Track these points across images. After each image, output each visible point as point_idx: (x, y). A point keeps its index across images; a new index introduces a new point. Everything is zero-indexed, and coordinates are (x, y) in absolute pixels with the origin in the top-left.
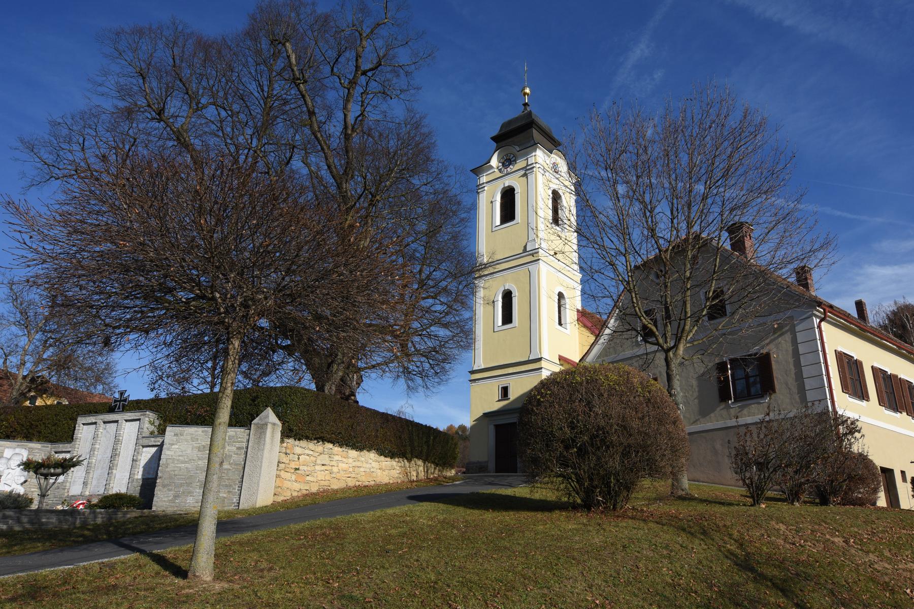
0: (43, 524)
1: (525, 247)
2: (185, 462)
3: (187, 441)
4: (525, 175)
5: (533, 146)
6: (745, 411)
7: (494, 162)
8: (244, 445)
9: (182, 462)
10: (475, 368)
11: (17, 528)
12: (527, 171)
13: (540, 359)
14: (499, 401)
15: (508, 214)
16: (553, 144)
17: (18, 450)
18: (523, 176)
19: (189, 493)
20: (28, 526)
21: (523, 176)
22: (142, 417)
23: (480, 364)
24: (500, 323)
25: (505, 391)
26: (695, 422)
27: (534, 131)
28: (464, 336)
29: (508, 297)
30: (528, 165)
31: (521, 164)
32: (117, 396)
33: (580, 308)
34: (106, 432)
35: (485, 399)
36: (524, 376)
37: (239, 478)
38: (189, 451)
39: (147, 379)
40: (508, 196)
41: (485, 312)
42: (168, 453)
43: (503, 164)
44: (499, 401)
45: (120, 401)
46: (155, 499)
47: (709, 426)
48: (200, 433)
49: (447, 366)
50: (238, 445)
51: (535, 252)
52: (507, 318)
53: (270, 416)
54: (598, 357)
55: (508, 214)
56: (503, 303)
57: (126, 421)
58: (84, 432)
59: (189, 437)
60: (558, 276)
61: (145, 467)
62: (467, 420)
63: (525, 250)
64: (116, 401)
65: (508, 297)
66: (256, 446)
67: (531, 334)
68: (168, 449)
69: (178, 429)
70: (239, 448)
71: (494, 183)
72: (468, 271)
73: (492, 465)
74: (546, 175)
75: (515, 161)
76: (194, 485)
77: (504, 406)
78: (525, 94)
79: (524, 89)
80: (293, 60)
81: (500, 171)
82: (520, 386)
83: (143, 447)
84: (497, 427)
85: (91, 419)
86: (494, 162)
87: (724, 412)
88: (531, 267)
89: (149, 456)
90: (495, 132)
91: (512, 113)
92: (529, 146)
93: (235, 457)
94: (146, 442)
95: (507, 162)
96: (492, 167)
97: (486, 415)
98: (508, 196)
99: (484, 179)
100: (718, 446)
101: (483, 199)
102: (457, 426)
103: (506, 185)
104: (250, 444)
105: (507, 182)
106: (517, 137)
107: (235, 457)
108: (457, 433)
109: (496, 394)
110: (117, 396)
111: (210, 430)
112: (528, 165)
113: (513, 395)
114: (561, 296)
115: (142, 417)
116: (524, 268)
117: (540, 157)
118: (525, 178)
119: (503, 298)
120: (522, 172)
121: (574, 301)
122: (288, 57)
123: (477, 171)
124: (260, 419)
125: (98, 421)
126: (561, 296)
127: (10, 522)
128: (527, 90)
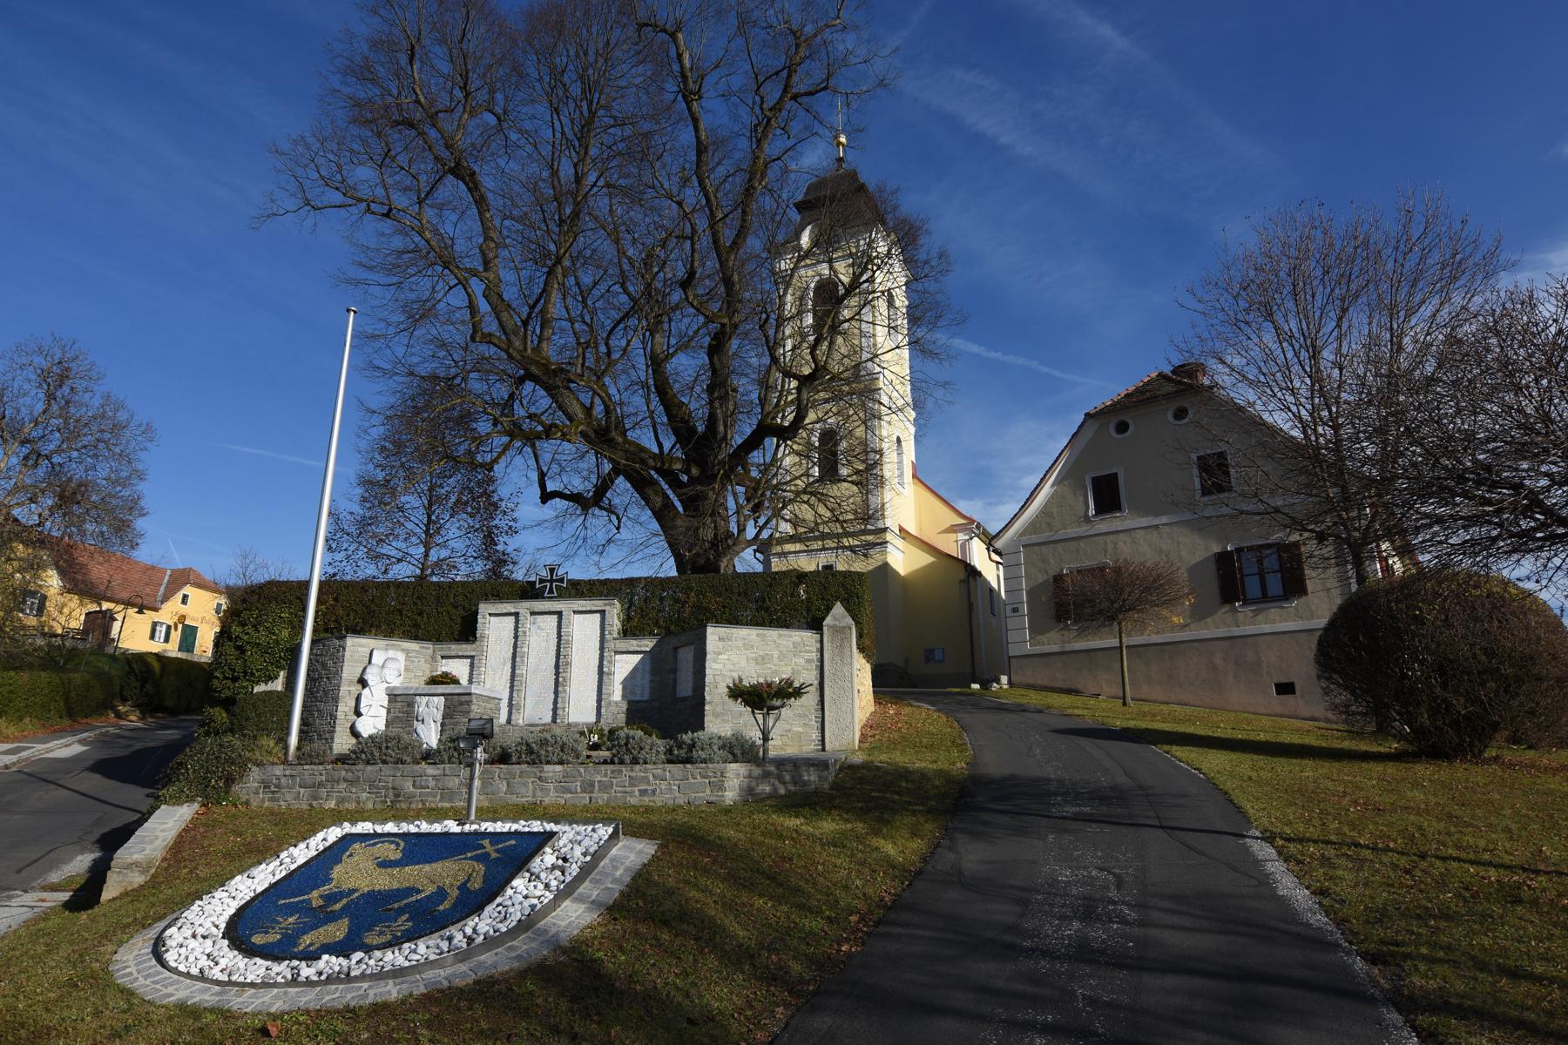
0: (805, 783)
6: (1260, 617)
17: (391, 653)
32: (544, 573)
34: (540, 633)
38: (743, 663)
42: (715, 666)
45: (551, 581)
47: (1205, 634)
53: (838, 615)
58: (495, 627)
59: (740, 643)
64: (541, 581)
66: (837, 659)
70: (808, 661)
78: (839, 143)
79: (837, 137)
83: (617, 653)
87: (1229, 618)
89: (630, 667)
100: (1218, 661)
104: (826, 655)
110: (544, 573)
111: (807, 637)
122: (680, 56)
124: (835, 619)
125: (522, 611)
126: (899, 440)
128: (843, 139)
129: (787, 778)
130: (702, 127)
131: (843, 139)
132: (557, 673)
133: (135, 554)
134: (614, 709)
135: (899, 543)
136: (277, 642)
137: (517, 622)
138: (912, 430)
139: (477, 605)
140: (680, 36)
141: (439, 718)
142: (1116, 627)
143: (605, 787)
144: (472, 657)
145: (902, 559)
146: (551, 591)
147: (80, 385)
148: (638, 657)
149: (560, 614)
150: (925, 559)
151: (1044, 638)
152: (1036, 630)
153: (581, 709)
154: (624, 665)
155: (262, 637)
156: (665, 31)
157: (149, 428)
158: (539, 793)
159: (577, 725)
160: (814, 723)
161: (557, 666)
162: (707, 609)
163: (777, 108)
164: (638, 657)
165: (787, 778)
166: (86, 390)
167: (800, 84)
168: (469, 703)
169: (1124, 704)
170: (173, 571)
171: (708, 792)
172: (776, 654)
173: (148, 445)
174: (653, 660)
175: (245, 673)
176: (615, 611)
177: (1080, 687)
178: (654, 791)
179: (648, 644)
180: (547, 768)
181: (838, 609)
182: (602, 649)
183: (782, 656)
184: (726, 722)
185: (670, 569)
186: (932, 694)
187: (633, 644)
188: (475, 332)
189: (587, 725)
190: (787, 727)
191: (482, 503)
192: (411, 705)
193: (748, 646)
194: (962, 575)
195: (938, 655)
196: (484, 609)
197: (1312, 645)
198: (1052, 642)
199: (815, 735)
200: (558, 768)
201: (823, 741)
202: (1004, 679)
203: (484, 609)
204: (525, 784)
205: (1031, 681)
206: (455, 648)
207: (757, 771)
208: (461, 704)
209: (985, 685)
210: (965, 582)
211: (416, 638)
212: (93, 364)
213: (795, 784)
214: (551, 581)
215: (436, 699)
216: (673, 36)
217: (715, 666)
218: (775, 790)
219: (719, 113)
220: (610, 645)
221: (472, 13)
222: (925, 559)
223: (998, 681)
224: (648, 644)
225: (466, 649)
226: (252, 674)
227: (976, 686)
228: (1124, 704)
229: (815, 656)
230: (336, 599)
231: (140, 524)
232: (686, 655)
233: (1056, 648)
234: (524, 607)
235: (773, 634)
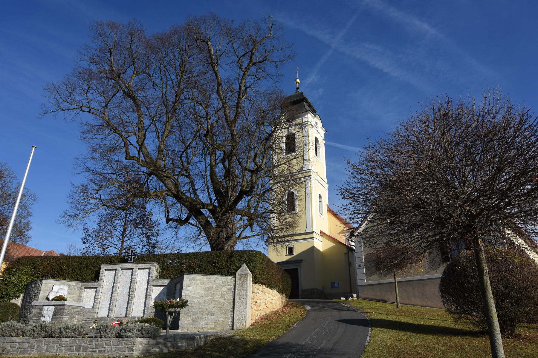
0: (179, 347)
2: (198, 298)
3: (197, 284)
5: (307, 112)
8: (232, 287)
9: (196, 298)
11: (165, 351)
12: (302, 126)
13: (313, 232)
16: (314, 112)
17: (62, 287)
19: (201, 318)
20: (171, 349)
22: (151, 267)
25: (291, 250)
26: (427, 273)
30: (303, 122)
31: (298, 121)
34: (124, 277)
37: (230, 307)
38: (199, 291)
39: (82, 236)
42: (186, 292)
44: (287, 255)
45: (131, 256)
46: (180, 322)
48: (205, 279)
50: (228, 287)
57: (139, 269)
58: (106, 275)
59: (198, 282)
61: (155, 299)
66: (241, 288)
68: (186, 290)
69: (191, 276)
70: (229, 289)
76: (204, 313)
78: (297, 82)
79: (296, 80)
80: (212, 51)
83: (154, 286)
85: (113, 267)
93: (227, 295)
94: (156, 283)
98: (291, 138)
107: (227, 295)
111: (229, 279)
113: (296, 252)
115: (151, 267)
117: (310, 117)
121: (326, 200)
122: (209, 50)
124: (242, 271)
125: (118, 269)
126: (320, 196)
127: (161, 346)
128: (298, 81)
129: (169, 345)
130: (219, 76)
131: (298, 81)
132: (129, 295)
133: (28, 245)
134: (150, 310)
135: (321, 238)
136: (21, 282)
137: (132, 272)
138: (327, 192)
139: (100, 266)
140: (209, 43)
141: (51, 315)
142: (393, 274)
143: (85, 349)
144: (96, 288)
145: (321, 245)
146: (131, 260)
147: (7, 180)
148: (162, 288)
149: (132, 269)
150: (330, 244)
151: (372, 278)
152: (369, 274)
153: (137, 311)
154: (156, 291)
155: (15, 280)
156: (204, 41)
157: (35, 196)
158: (58, 351)
159: (135, 317)
160: (230, 317)
161: (129, 292)
162: (193, 267)
163: (247, 68)
164: (162, 288)
165: (169, 345)
166: (10, 182)
167: (255, 58)
168: (63, 309)
169: (397, 307)
170: (46, 252)
171: (127, 351)
172: (214, 286)
173: (34, 202)
174: (168, 289)
175: (7, 295)
176: (155, 268)
177: (386, 299)
178: (104, 351)
179: (166, 282)
180: (63, 339)
181: (244, 266)
182: (148, 284)
183: (217, 287)
184: (189, 316)
185: (207, 248)
186: (324, 302)
187: (161, 282)
188: (127, 156)
189: (138, 318)
190: (217, 319)
191: (145, 223)
192: (41, 309)
193: (202, 283)
194: (345, 251)
195: (336, 285)
196: (103, 267)
197: (439, 281)
198: (375, 280)
199: (230, 322)
200: (68, 340)
201: (233, 325)
202: (355, 295)
203: (103, 267)
204: (54, 347)
205: (367, 296)
206: (90, 284)
207: (152, 342)
208: (61, 310)
209: (347, 299)
210: (347, 254)
211: (77, 280)
212: (13, 172)
213: (173, 347)
214: (131, 256)
215: (51, 307)
216: (207, 43)
217: (186, 292)
218: (162, 351)
219: (226, 72)
220: (151, 283)
221: (135, 40)
222: (330, 244)
223: (352, 297)
224: (166, 282)
225: (94, 284)
226: (10, 295)
227: (343, 299)
228: (397, 307)
229: (232, 287)
230: (48, 264)
231: (29, 233)
232: (178, 286)
233: (376, 282)
234: (119, 266)
235: (214, 278)
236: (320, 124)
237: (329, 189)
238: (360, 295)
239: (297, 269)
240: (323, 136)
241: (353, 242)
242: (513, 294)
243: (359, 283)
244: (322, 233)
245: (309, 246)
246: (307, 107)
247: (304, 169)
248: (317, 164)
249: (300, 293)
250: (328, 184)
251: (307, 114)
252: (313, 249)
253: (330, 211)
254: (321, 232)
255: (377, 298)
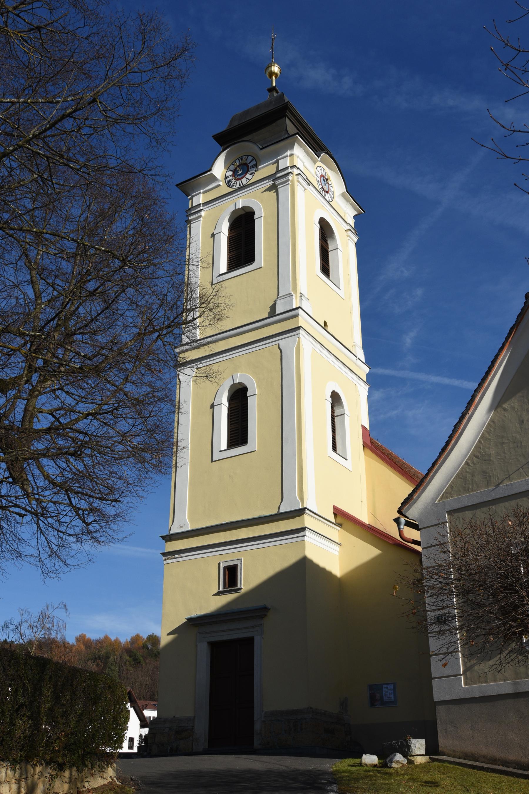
1: (273, 307)
4: (274, 188)
7: (219, 169)
10: (175, 530)
12: (277, 181)
13: (301, 512)
14: (219, 593)
15: (242, 251)
16: (317, 147)
18: (269, 189)
21: (269, 189)
23: (184, 521)
24: (224, 445)
25: (231, 574)
27: (288, 122)
28: (157, 450)
29: (239, 397)
30: (278, 171)
31: (266, 170)
33: (367, 426)
35: (191, 591)
36: (269, 544)
40: (243, 227)
41: (197, 406)
43: (235, 172)
44: (219, 593)
49: (110, 509)
51: (293, 313)
52: (238, 435)
54: (447, 494)
55: (242, 251)
56: (230, 409)
60: (328, 363)
62: (162, 625)
63: (272, 312)
65: (239, 397)
67: (284, 465)
71: (218, 204)
72: (169, 318)
73: (202, 728)
74: (310, 196)
75: (256, 166)
77: (229, 604)
78: (272, 74)
81: (229, 184)
82: (259, 566)
84: (214, 646)
86: (219, 169)
88: (284, 342)
90: (222, 127)
91: (250, 100)
92: (281, 141)
95: (242, 168)
96: (214, 179)
97: (195, 623)
98: (243, 227)
99: (200, 199)
101: (198, 231)
102: (145, 637)
103: (240, 205)
105: (241, 201)
106: (257, 132)
108: (145, 646)
109: (214, 580)
112: (278, 171)
113: (247, 581)
114: (336, 398)
116: (271, 345)
118: (273, 193)
119: (231, 400)
120: (269, 183)
121: (358, 413)
123: (187, 187)
126: (336, 398)
128: (276, 69)
131: (276, 69)
135: (335, 533)
138: (364, 390)
145: (334, 554)
195: (388, 693)
202: (418, 746)
205: (470, 748)
209: (385, 757)
223: (406, 751)
227: (370, 759)
236: (337, 185)
237: (372, 381)
238: (443, 742)
239: (250, 641)
240: (352, 221)
241: (416, 527)
242: (134, 469)
243: (440, 692)
244: (342, 517)
245: (291, 559)
246: (291, 128)
247: (279, 309)
248: (331, 304)
249: (257, 726)
250: (367, 362)
251: (292, 147)
252: (304, 565)
253: (372, 444)
254: (338, 512)
255: (513, 756)
